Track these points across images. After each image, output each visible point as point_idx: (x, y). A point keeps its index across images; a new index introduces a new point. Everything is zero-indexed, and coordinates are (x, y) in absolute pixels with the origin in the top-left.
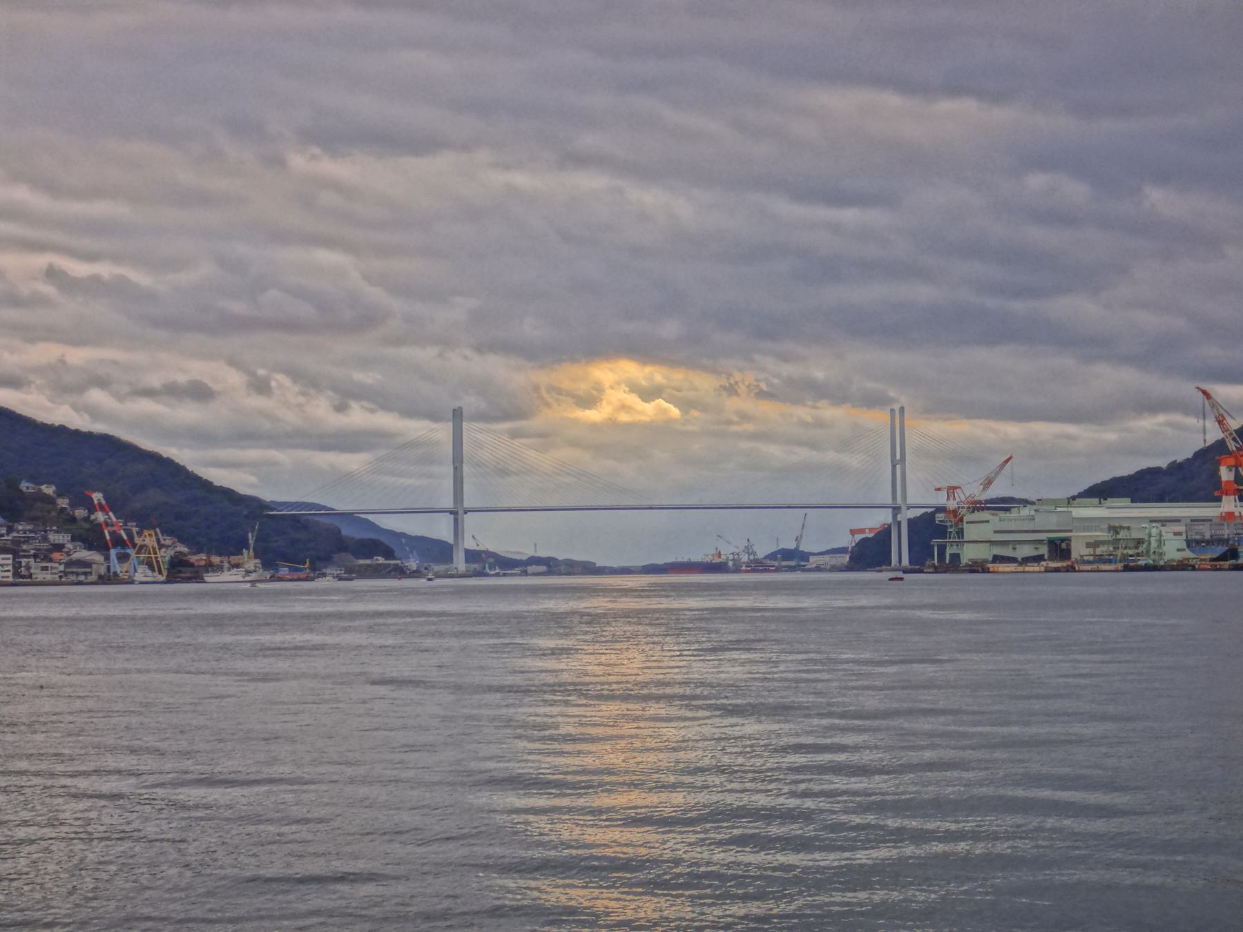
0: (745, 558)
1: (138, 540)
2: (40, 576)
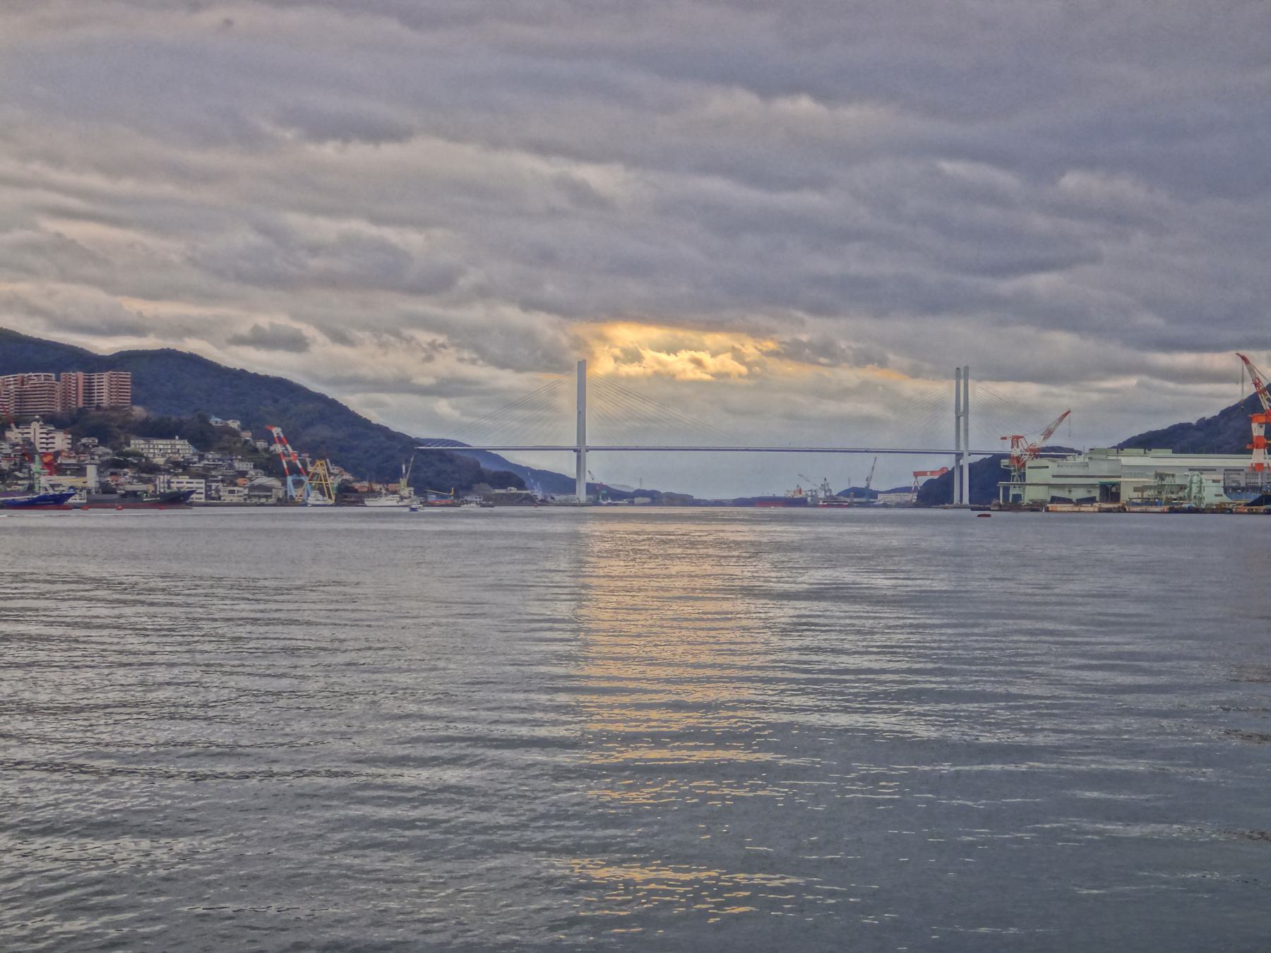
0: (822, 495)
1: (310, 469)
2: (227, 498)
